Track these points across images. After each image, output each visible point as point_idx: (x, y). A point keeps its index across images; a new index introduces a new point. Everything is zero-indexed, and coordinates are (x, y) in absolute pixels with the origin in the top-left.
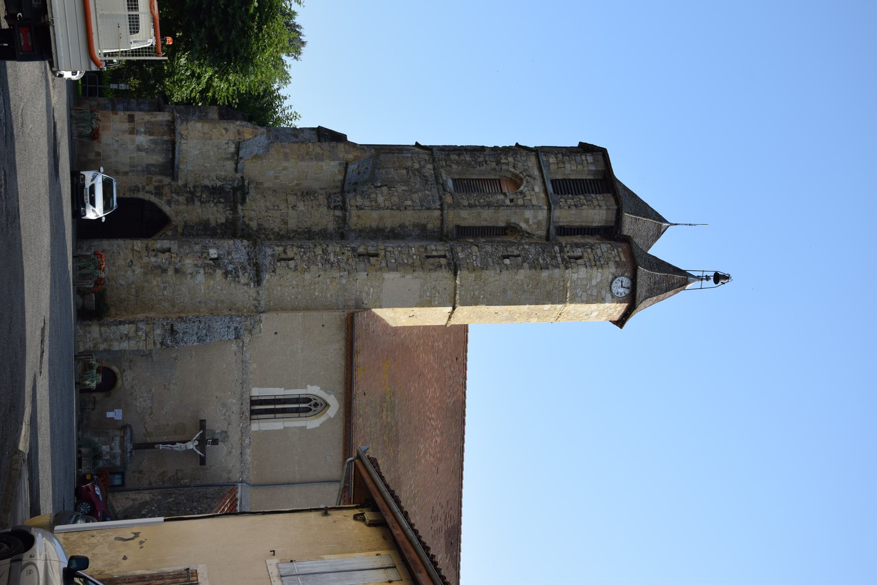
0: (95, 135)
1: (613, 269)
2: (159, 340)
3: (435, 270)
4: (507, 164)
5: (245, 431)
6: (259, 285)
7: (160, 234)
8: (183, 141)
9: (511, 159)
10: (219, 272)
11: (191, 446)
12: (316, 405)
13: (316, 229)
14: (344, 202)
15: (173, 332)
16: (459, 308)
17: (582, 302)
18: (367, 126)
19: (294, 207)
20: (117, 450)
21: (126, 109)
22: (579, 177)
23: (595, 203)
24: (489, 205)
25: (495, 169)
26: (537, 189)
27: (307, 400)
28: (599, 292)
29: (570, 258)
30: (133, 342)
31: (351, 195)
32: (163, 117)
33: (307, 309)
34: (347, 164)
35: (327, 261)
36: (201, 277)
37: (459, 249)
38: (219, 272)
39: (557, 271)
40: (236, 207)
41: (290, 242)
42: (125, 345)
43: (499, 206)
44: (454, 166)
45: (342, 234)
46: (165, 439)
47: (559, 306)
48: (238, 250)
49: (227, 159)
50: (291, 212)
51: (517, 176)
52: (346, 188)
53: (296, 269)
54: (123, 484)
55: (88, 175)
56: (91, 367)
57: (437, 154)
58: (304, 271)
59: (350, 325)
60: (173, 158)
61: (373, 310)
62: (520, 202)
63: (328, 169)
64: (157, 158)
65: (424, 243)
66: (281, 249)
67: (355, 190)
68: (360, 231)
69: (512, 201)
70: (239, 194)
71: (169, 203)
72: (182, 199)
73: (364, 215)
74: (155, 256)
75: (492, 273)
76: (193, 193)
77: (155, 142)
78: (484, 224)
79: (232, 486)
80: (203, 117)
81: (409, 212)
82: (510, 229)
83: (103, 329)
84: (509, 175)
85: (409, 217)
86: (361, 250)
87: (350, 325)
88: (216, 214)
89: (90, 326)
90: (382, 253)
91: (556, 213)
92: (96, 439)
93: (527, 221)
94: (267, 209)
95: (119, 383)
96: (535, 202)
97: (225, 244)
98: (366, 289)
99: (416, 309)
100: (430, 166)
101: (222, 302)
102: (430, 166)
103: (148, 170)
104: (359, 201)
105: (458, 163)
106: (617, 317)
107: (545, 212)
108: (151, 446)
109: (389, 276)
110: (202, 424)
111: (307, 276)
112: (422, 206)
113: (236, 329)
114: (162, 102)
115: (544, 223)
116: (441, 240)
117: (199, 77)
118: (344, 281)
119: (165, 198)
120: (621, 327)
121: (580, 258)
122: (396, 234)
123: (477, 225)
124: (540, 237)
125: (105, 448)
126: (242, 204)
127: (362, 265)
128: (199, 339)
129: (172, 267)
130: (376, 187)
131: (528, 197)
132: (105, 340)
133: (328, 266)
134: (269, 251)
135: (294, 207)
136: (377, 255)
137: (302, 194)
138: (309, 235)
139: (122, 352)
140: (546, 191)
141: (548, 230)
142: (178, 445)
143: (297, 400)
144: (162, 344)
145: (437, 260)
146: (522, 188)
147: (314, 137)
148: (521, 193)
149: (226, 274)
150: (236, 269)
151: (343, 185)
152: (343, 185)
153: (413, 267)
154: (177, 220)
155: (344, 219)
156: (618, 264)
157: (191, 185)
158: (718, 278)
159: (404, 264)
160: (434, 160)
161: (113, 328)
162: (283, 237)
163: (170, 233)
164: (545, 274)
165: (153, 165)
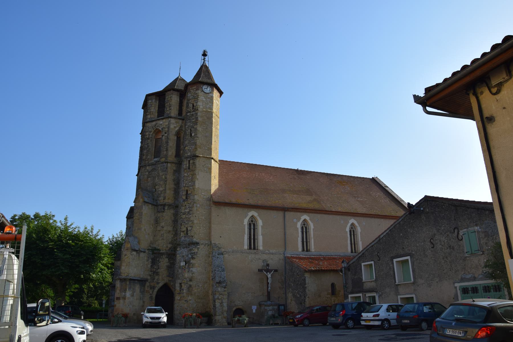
0: (126, 316)
1: (199, 91)
2: (223, 289)
3: (195, 165)
4: (149, 135)
5: (263, 253)
6: (198, 243)
7: (172, 288)
8: (130, 275)
9: (147, 134)
10: (192, 261)
11: (269, 276)
12: (252, 221)
13: (173, 218)
14: (161, 205)
15: (220, 283)
16: (213, 156)
17: (212, 105)
18: (128, 197)
19: (163, 227)
20: (271, 308)
21: (114, 301)
22: (157, 107)
23: (169, 99)
24: (167, 142)
25: (151, 140)
26: (161, 123)
27: (250, 225)
28: (209, 98)
29: (193, 108)
30: (224, 301)
31: (158, 202)
32: (118, 284)
33: (210, 223)
34: (145, 202)
35: (188, 212)
36: (194, 270)
37: (186, 155)
38: (192, 261)
39: (198, 114)
40: (161, 253)
41: (179, 230)
42: (225, 305)
43: (168, 138)
44: (149, 157)
45: (176, 207)
46: (265, 287)
47: (214, 115)
48: (182, 252)
49: (139, 256)
50: (165, 229)
51: (155, 131)
52: (155, 204)
53: (192, 227)
54: (284, 305)
55: (145, 320)
56: (238, 320)
57: (142, 164)
58: (193, 223)
59: (219, 204)
60: (138, 280)
61: (212, 193)
62: (166, 129)
63: (146, 210)
64: (137, 288)
65: (182, 170)
66: (182, 233)
67: (156, 200)
68: (175, 199)
69: (166, 133)
70: (155, 252)
71: (158, 283)
72: (156, 277)
73: (168, 197)
74: (183, 290)
75: (198, 141)
76: (154, 272)
77: (130, 288)
78: (175, 145)
79: (286, 259)
80: (119, 267)
81: (168, 177)
82: (178, 134)
83: (217, 314)
84: (154, 135)
85: (170, 177)
86: (184, 198)
87: (219, 204)
88: (164, 262)
89: (215, 320)
90: (186, 188)
91: (172, 115)
92: (266, 317)
93: (175, 127)
94: (163, 239)
95: (241, 307)
96: (167, 124)
97: (179, 258)
98: (202, 196)
99: (212, 175)
100: (148, 168)
101: (206, 260)
102: (148, 168)
103: (142, 292)
104: (161, 198)
105: (147, 156)
106: (218, 94)
107: (172, 119)
108: (269, 293)
109: (197, 186)
110: (259, 270)
111: (195, 222)
112: (165, 171)
113: (218, 254)
114: (112, 286)
115: (177, 120)
116: (181, 164)
117: (102, 269)
118: (198, 205)
119: (156, 285)
120: (223, 93)
121: (193, 106)
122: (177, 183)
123: (175, 148)
124: (182, 123)
125: (270, 313)
126: (160, 250)
127: (191, 197)
128: (223, 270)
129: (189, 283)
130: (155, 191)
131: (165, 126)
132: (223, 313)
133: (191, 212)
134: (183, 239)
135: (163, 227)
136: (187, 191)
137: (157, 224)
138: (175, 221)
139: (228, 306)
140: (162, 119)
141: (179, 119)
142: (269, 281)
143: (250, 229)
144: (225, 288)
145: (191, 164)
146: (160, 129)
147: (131, 220)
148: (162, 129)
149: (193, 258)
150: (191, 254)
151: (154, 205)
152: (154, 205)
153: (194, 175)
154: (166, 280)
155: (169, 205)
156: (197, 89)
157: (150, 273)
158: (204, 55)
159: (192, 179)
160: (145, 166)
161: (217, 310)
162: (176, 233)
163: (172, 283)
164: (200, 119)
165: (140, 290)
